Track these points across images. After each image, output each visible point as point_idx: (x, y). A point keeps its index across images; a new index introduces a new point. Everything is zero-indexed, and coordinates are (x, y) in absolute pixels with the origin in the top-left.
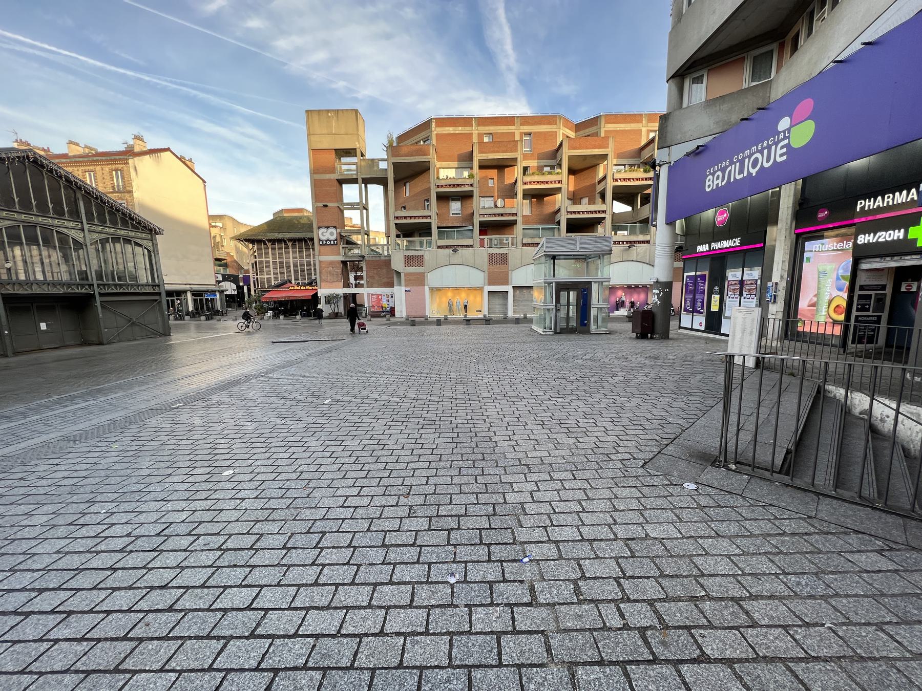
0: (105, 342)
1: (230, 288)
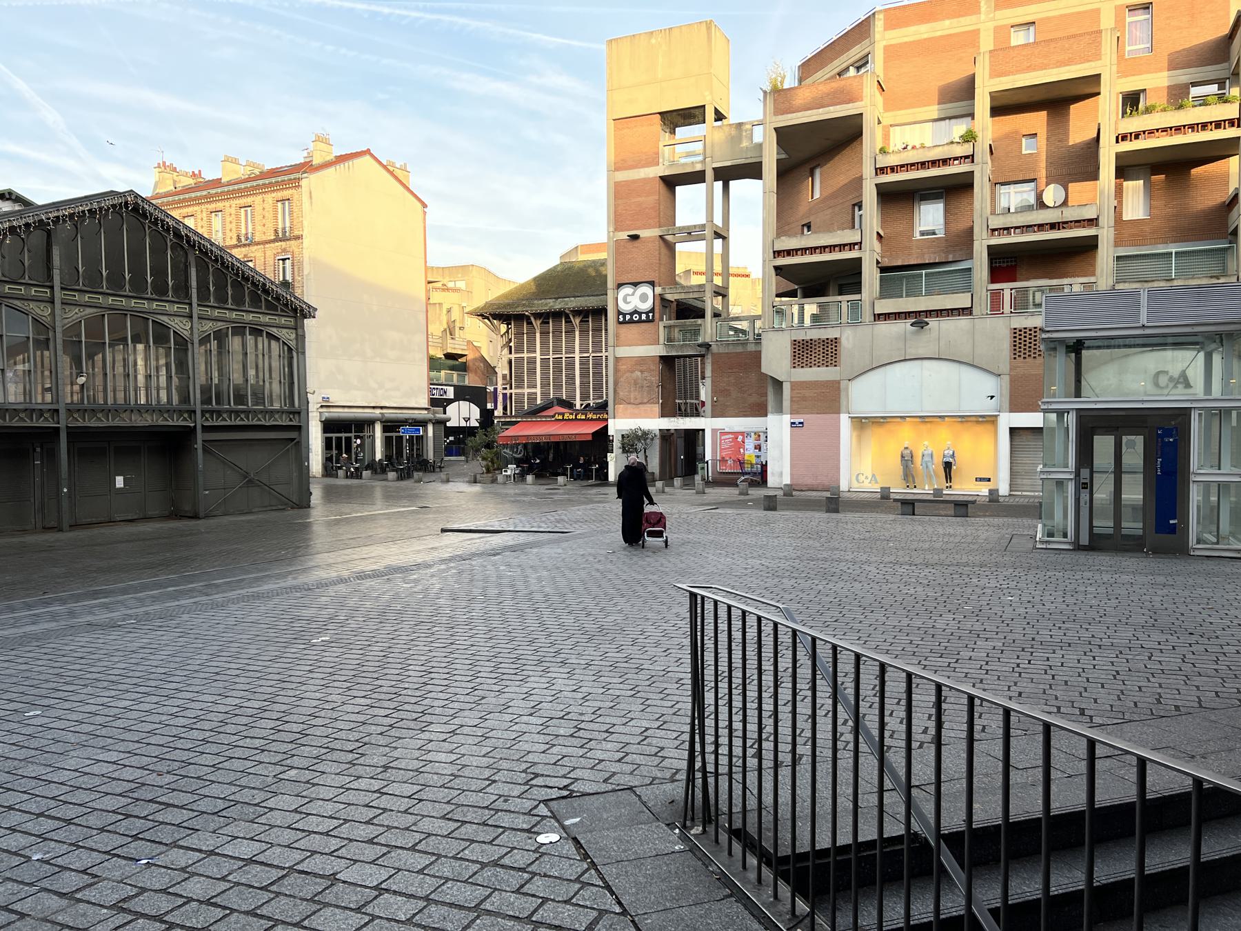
0: (202, 514)
1: (463, 414)
